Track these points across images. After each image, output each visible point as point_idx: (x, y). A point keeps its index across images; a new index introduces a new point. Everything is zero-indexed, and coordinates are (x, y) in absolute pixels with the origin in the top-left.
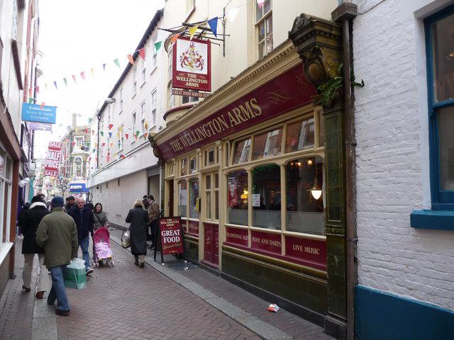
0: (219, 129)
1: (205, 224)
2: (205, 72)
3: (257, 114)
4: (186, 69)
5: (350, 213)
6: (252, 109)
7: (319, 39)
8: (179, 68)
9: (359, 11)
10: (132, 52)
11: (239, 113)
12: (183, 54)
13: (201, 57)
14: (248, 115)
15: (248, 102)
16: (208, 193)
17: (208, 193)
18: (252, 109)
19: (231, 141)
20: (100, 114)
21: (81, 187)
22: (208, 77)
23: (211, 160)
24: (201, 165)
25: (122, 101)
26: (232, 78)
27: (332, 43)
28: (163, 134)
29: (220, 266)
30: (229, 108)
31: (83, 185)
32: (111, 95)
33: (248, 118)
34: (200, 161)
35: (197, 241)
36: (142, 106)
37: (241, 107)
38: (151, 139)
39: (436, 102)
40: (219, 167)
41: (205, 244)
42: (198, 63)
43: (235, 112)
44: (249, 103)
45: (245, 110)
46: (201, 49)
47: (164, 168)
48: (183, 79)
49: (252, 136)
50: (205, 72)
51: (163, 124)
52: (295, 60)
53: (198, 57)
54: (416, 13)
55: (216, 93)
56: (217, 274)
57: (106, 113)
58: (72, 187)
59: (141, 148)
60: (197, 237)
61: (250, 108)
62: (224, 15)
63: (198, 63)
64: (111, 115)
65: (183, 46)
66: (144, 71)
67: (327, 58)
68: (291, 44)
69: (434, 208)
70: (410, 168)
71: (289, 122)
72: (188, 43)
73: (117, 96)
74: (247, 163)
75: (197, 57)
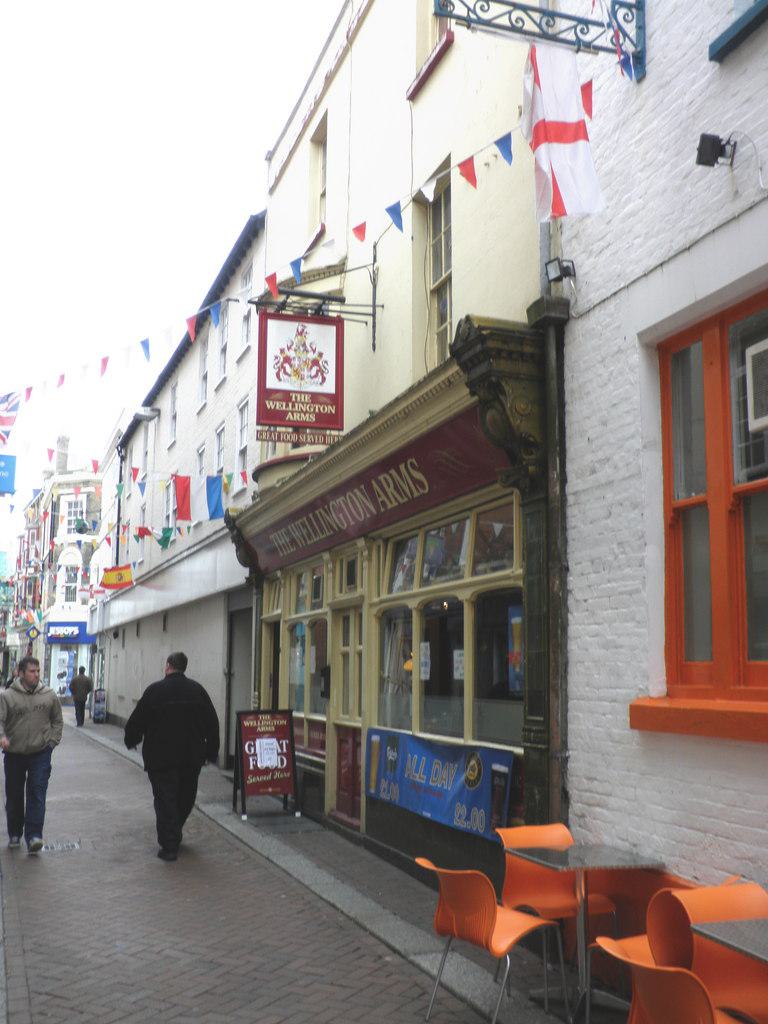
0: (360, 515)
1: (339, 728)
2: (330, 387)
3: (422, 491)
4: (286, 385)
5: (555, 703)
6: (412, 477)
7: (503, 365)
8: (272, 382)
9: (573, 313)
10: (194, 308)
11: (392, 485)
12: (282, 351)
13: (321, 355)
14: (407, 491)
15: (343, 498)
16: (346, 656)
17: (346, 656)
18: (412, 477)
19: (386, 541)
20: (125, 443)
21: (76, 630)
22: (337, 399)
23: (351, 580)
24: (334, 592)
25: (174, 417)
26: (371, 412)
27: (524, 368)
28: (252, 514)
29: (362, 823)
30: (322, 501)
31: (82, 626)
32: (150, 401)
33: (407, 496)
34: (365, 572)
35: (322, 766)
36: (219, 435)
37: (393, 472)
38: (231, 522)
39: (681, 498)
40: (362, 597)
41: (339, 771)
42: (315, 369)
43: (383, 480)
44: (406, 467)
45: (398, 478)
46: (321, 337)
47: (260, 592)
48: (279, 406)
49: (473, 515)
50: (330, 387)
51: (253, 487)
52: (461, 399)
53: (315, 356)
54: (640, 335)
55: (354, 432)
56: (358, 842)
57: (138, 445)
58: (53, 631)
59: (208, 544)
60: (323, 757)
61: (408, 477)
62: (375, 260)
63: (315, 369)
64: (150, 450)
65: (281, 333)
66: (224, 350)
67: (517, 402)
68: (456, 368)
69: (670, 695)
70: (633, 619)
71: (482, 509)
72: (292, 327)
73: (164, 403)
74: (413, 593)
75: (311, 356)
